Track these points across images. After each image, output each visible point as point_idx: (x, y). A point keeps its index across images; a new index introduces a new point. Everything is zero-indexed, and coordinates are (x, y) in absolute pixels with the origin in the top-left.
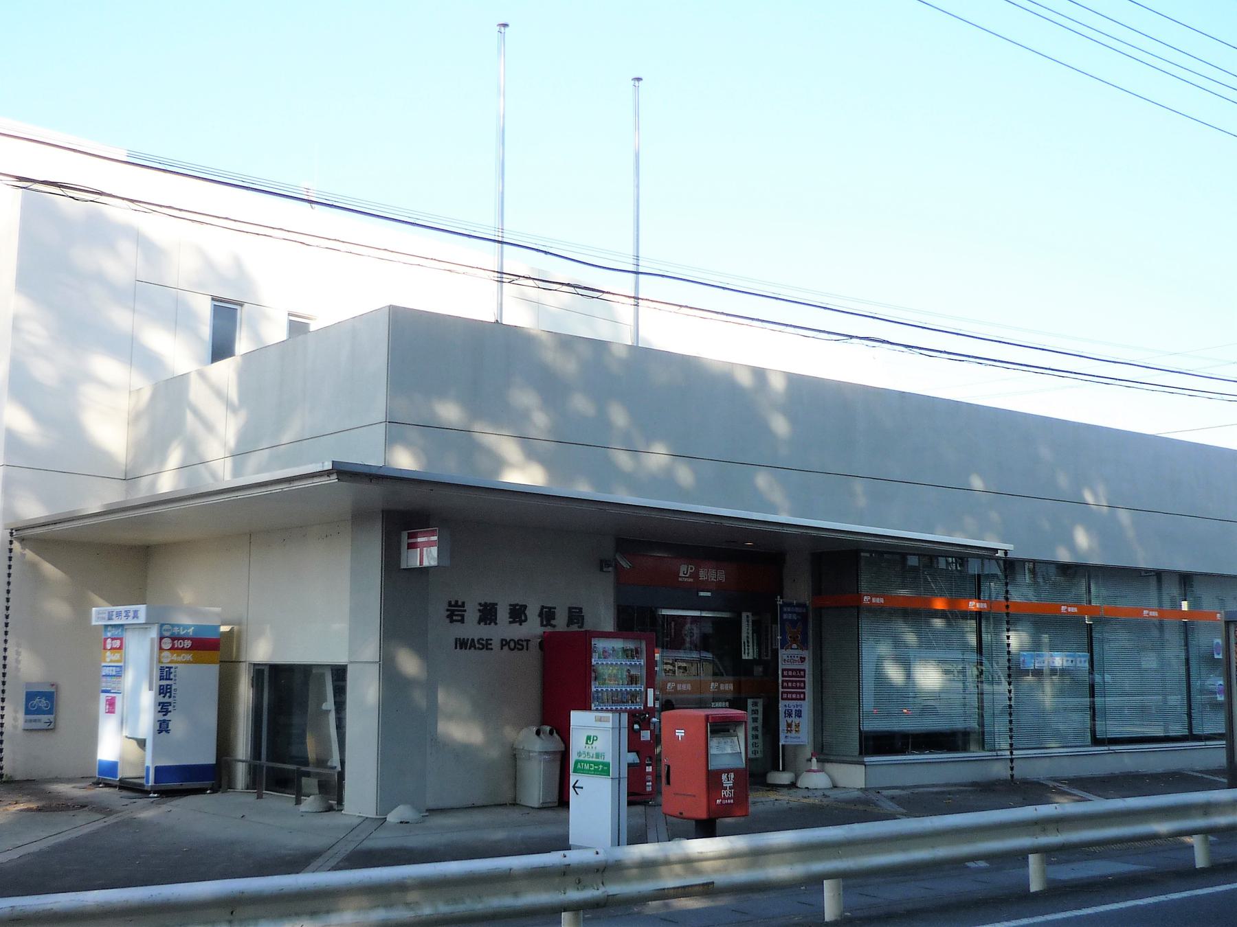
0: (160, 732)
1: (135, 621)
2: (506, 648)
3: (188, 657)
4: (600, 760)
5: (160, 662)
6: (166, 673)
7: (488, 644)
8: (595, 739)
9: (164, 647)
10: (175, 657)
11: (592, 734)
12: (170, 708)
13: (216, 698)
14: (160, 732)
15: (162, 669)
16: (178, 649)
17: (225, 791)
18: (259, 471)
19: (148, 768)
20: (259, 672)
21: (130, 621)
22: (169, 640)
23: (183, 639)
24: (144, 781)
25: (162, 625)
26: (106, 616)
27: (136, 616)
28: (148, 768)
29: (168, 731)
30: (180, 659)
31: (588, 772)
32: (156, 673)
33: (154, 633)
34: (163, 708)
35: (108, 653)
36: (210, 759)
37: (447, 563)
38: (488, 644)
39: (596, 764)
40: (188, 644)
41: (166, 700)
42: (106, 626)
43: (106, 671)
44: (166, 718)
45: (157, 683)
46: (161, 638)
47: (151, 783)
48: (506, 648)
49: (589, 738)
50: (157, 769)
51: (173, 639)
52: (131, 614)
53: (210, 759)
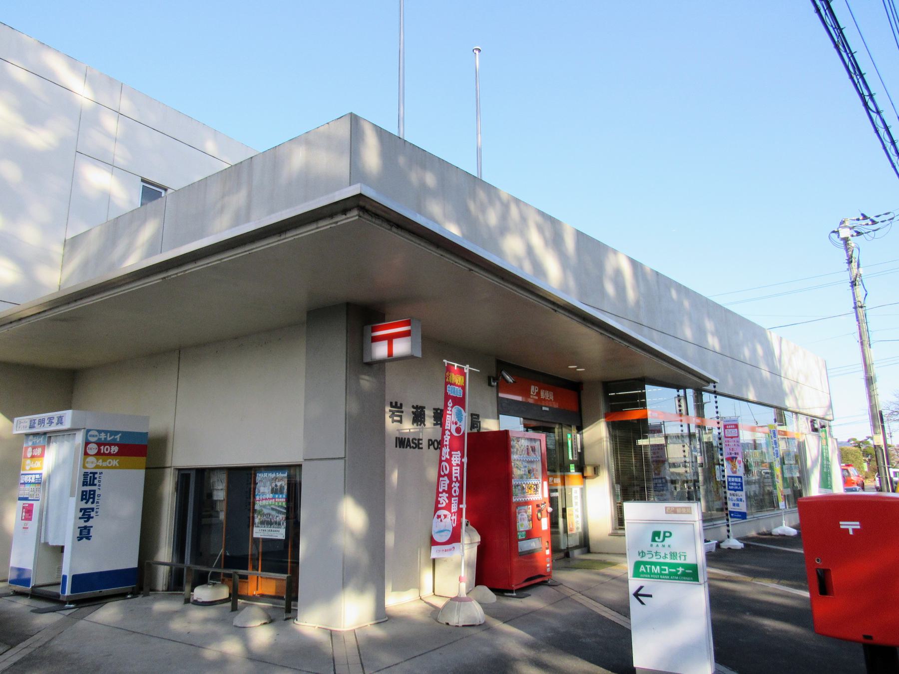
0: (80, 539)
1: (60, 427)
2: (432, 447)
3: (115, 462)
4: (678, 561)
5: (84, 467)
6: (89, 479)
7: (419, 444)
8: (668, 534)
9: (89, 452)
10: (100, 463)
11: (662, 528)
12: (93, 514)
13: (386, 497)
14: (80, 539)
15: (86, 475)
16: (104, 454)
17: (146, 595)
18: (236, 222)
19: (65, 577)
20: (184, 475)
21: (54, 427)
22: (95, 446)
23: (110, 445)
24: (58, 590)
25: (88, 431)
26: (28, 424)
27: (60, 420)
28: (65, 577)
29: (88, 538)
30: (105, 464)
31: (659, 576)
32: (79, 479)
33: (79, 438)
34: (86, 514)
35: (28, 461)
36: (134, 564)
37: (419, 354)
38: (419, 444)
39: (670, 565)
40: (115, 449)
41: (89, 505)
42: (27, 435)
43: (26, 479)
44: (88, 524)
45: (79, 488)
46: (87, 443)
47: (68, 592)
48: (432, 447)
49: (656, 534)
50: (75, 578)
51: (99, 444)
52: (55, 421)
53: (134, 564)
